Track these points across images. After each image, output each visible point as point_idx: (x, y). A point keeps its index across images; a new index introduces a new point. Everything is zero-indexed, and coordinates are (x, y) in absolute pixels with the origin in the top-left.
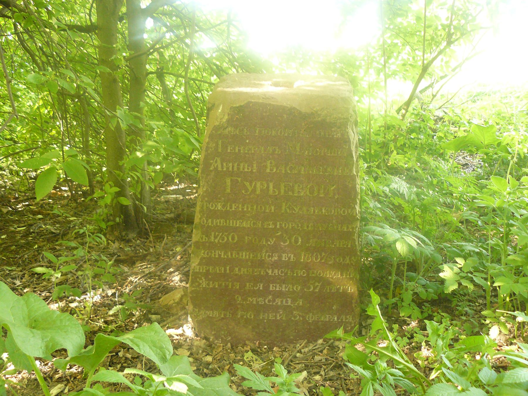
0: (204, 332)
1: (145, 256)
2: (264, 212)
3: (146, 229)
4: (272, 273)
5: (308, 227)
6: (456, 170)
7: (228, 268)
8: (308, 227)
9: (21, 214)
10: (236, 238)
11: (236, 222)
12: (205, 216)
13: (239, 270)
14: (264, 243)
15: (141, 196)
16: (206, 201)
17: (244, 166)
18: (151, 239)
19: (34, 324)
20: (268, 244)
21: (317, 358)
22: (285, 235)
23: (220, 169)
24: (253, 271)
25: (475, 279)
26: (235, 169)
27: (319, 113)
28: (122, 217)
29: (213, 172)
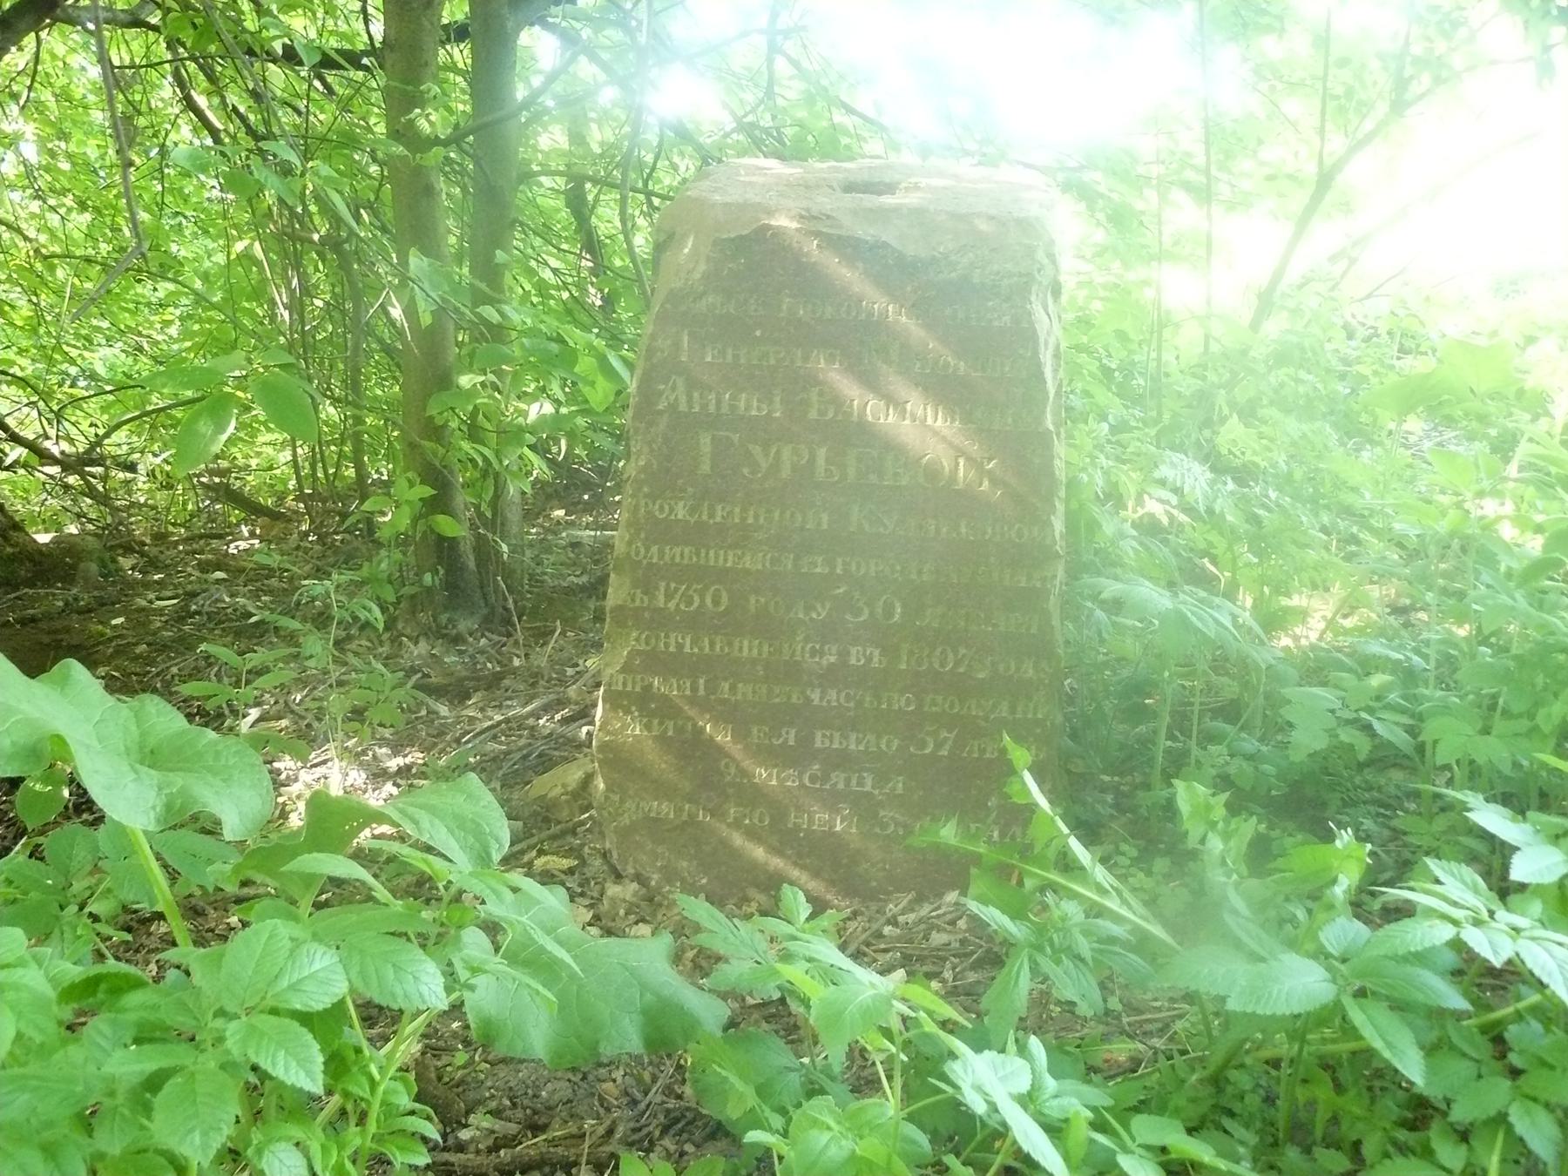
0: (635, 861)
1: (498, 678)
2: (802, 529)
3: (506, 609)
4: (821, 699)
5: (920, 572)
6: (1409, 472)
7: (702, 681)
8: (920, 572)
9: (141, 506)
11: (726, 554)
12: (643, 535)
13: (733, 688)
14: (801, 616)
15: (494, 514)
16: (646, 496)
17: (747, 400)
18: (520, 636)
19: (152, 756)
20: (811, 619)
21: (938, 938)
22: (857, 595)
23: (683, 407)
25: (1377, 726)
27: (953, 258)
28: (442, 572)
29: (666, 416)
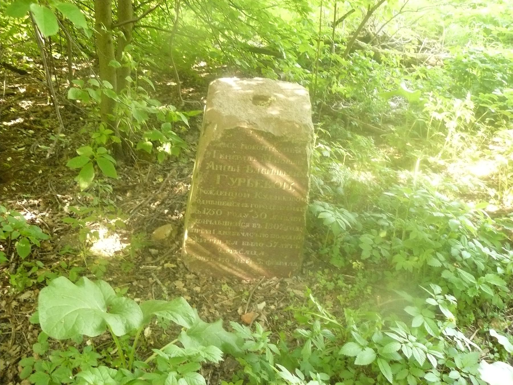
2: (243, 197)
5: (272, 207)
8: (272, 207)
10: (221, 213)
18: (137, 166)
21: (272, 292)
23: (213, 168)
24: (231, 233)
26: (224, 169)
